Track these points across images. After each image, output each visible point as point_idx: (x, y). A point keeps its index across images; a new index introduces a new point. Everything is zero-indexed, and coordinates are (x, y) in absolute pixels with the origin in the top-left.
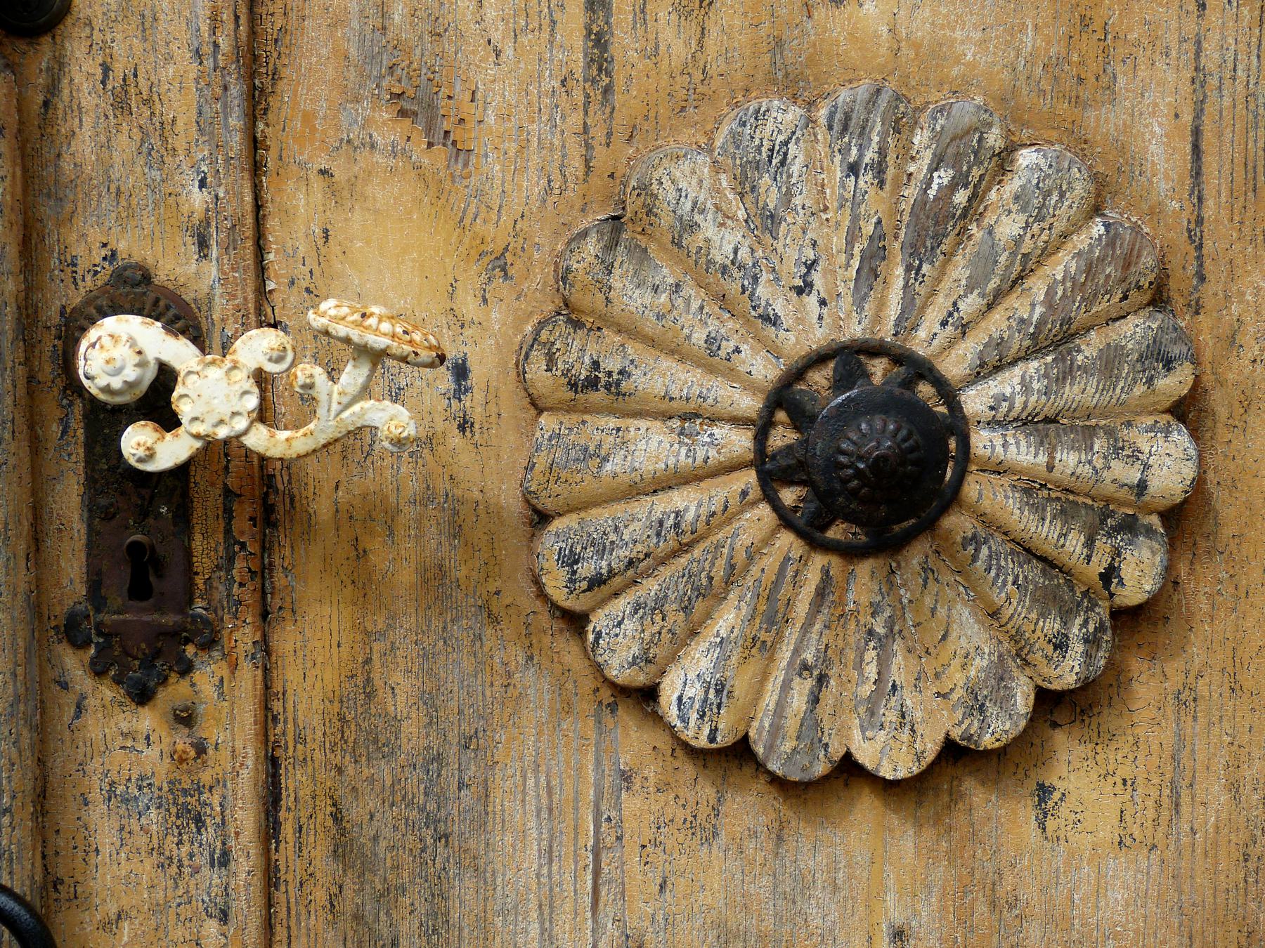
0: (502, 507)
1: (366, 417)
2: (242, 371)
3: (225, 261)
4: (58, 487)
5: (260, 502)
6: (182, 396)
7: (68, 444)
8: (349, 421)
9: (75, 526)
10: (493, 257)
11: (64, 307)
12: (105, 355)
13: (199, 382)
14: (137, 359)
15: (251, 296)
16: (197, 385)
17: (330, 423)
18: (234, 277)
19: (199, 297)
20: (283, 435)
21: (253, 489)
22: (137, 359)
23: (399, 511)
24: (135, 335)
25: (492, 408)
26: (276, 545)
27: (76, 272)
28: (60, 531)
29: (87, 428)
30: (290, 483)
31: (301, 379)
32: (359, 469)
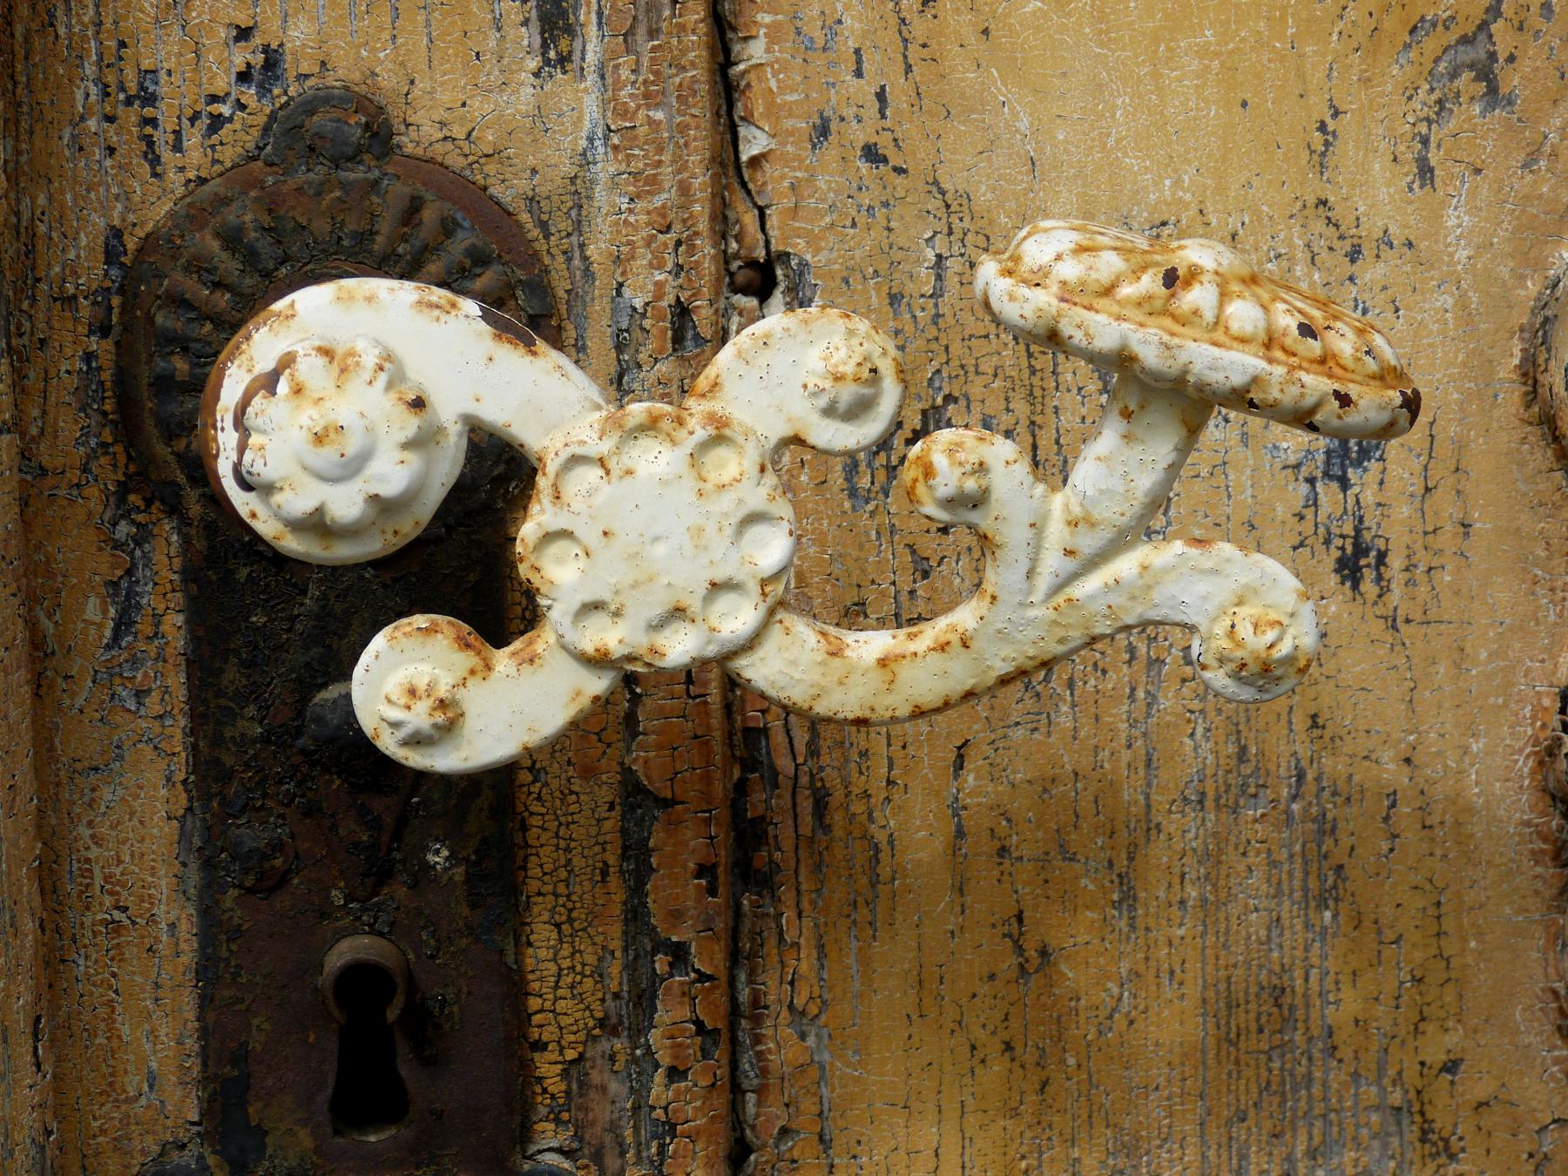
0: (1469, 809)
1: (1156, 596)
2: (741, 451)
3: (625, 73)
4: (106, 794)
5: (722, 813)
6: (549, 537)
7: (135, 662)
8: (1100, 606)
9: (160, 911)
10: (1453, 37)
11: (117, 233)
12: (309, 417)
13: (606, 491)
14: (410, 425)
15: (700, 181)
16: (599, 499)
17: (1032, 613)
18: (651, 122)
19: (543, 191)
20: (870, 645)
21: (707, 779)
22: (410, 425)
23: (1152, 829)
24: (401, 350)
25: (1445, 507)
26: (772, 942)
27: (153, 122)
28: (114, 927)
29: (196, 611)
30: (813, 751)
31: (948, 479)
32: (1029, 703)
